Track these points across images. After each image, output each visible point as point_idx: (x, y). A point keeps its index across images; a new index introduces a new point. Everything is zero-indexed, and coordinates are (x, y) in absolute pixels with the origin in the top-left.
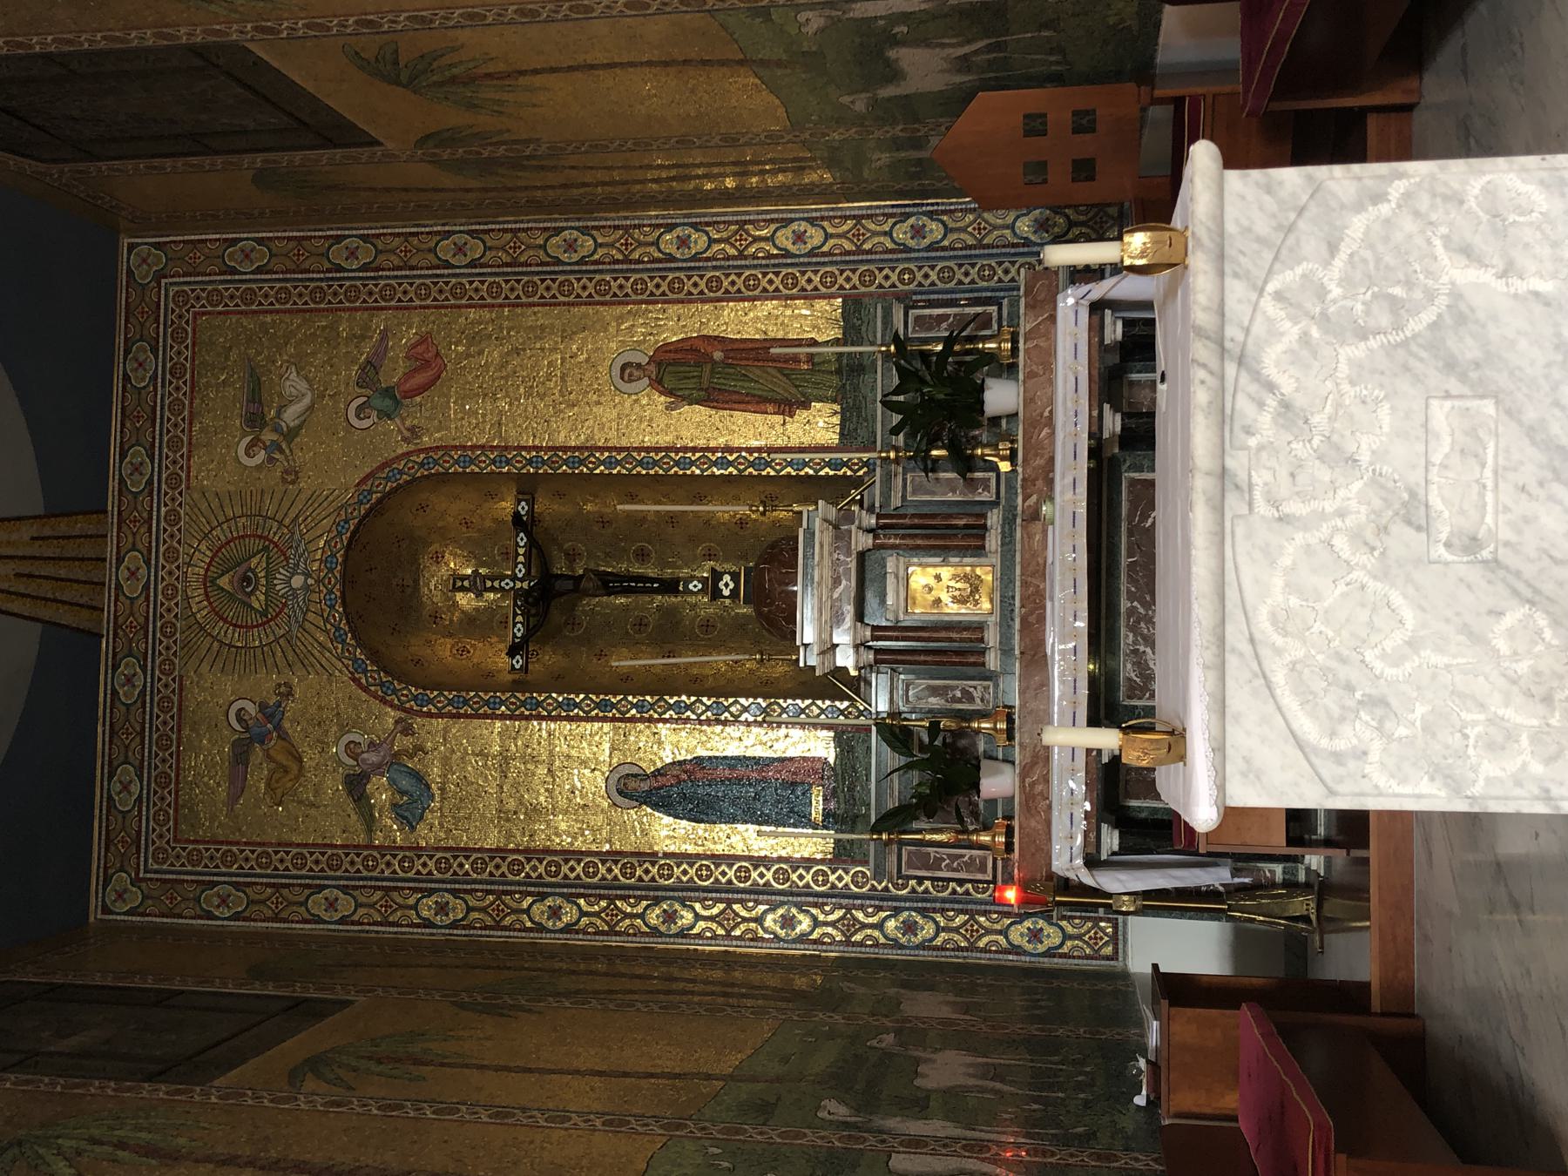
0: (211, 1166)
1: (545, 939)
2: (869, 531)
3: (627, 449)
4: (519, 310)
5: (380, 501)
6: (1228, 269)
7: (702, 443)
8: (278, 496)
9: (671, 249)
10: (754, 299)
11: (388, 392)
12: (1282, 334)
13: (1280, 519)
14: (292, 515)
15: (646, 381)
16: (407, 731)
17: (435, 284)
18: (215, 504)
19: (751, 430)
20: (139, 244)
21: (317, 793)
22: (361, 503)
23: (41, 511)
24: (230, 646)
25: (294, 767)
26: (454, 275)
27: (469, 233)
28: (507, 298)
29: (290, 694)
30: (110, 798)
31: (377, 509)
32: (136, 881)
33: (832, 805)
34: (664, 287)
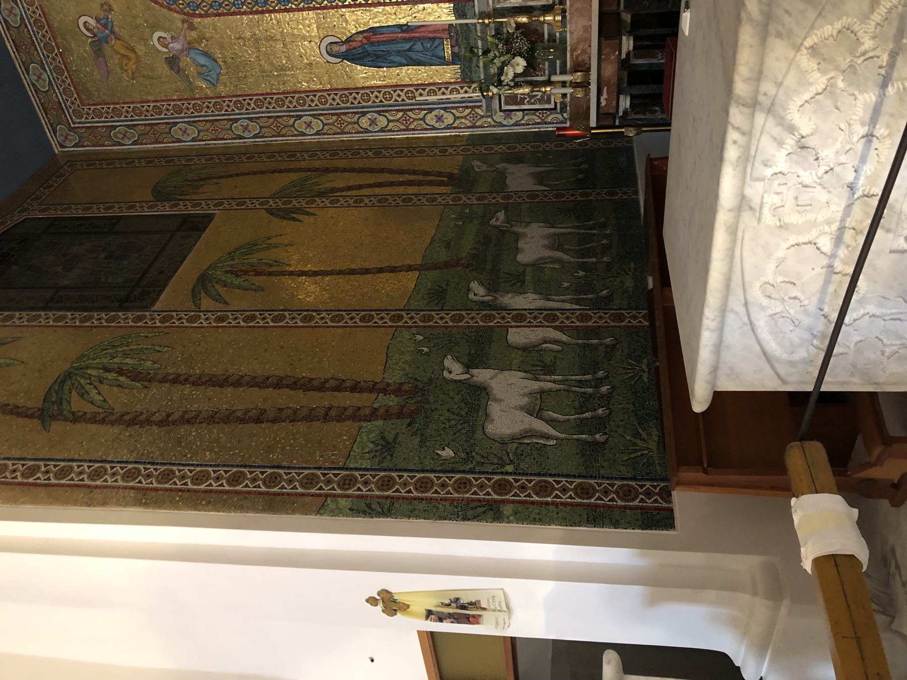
0: (167, 385)
1: (307, 139)
6: (772, 29)
12: (811, 84)
13: (781, 227)
16: (192, 27)
21: (152, 70)
25: (132, 55)
29: (111, 10)
30: (33, 85)
33: (456, 49)
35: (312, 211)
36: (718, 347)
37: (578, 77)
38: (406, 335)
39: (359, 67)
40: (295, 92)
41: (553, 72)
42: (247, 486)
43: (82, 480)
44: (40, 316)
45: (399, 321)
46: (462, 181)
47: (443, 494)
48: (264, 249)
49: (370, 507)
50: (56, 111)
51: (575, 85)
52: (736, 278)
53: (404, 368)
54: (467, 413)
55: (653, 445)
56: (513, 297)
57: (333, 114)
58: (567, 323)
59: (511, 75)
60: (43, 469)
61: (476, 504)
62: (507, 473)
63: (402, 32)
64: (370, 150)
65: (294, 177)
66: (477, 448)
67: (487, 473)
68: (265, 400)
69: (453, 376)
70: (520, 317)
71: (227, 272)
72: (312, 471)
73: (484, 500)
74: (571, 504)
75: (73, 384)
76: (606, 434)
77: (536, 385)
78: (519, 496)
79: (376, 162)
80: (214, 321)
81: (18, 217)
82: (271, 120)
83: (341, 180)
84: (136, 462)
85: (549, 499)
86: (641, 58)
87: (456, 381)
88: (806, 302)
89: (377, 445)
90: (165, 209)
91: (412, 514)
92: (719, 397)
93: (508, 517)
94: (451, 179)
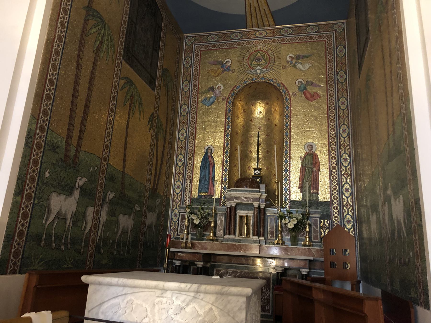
0: (93, 60)
1: (177, 133)
2: (259, 206)
3: (290, 147)
4: (327, 119)
5: (278, 88)
6: (219, 295)
7: (292, 165)
8: (280, 65)
9: (344, 157)
10: (330, 178)
11: (305, 88)
12: (201, 309)
13: (154, 304)
14: (275, 68)
15: (308, 151)
16: (223, 100)
17: (334, 98)
18: (278, 50)
19: (295, 177)
20: (344, 25)
21: (210, 80)
22: (277, 84)
23: (271, 11)
24: (244, 58)
26: (336, 102)
27: (348, 105)
28: (330, 116)
29: (232, 72)
30: (210, 35)
31: (276, 88)
32: (192, 43)
33: (203, 197)
34: (333, 155)
35: (151, 131)
36: (110, 285)
37: (189, 245)
38: (98, 163)
39: (201, 159)
40: (196, 132)
41: (192, 235)
42: (48, 86)
43: (61, 18)
44: (127, 15)
45: (104, 160)
46: (154, 193)
47: (30, 170)
48: (139, 109)
49: (30, 137)
50: (200, 40)
51: (186, 243)
52: (137, 290)
53: (84, 160)
54: (62, 185)
55: (36, 267)
56: (106, 211)
57: (185, 145)
58: (92, 233)
59: (193, 218)
60: (68, 3)
61: (24, 185)
62: (34, 200)
63: (212, 177)
64: (170, 158)
65: (164, 125)
66: (47, 188)
67: (36, 191)
68: (81, 100)
69: (78, 181)
70: (98, 213)
71: (133, 92)
72: (49, 115)
73: (25, 189)
74: (16, 228)
75: (99, 22)
76: (44, 246)
77: (69, 217)
78: (24, 204)
79: (165, 159)
80: (115, 84)
81: (163, 14)
82: (186, 121)
83: (160, 143)
84: (64, 42)
85: (20, 218)
86: (193, 270)
87: (76, 182)
88: (123, 316)
89: (55, 144)
90: (159, 73)
91: (24, 155)
92: (86, 286)
93: (15, 198)
94: (155, 189)
